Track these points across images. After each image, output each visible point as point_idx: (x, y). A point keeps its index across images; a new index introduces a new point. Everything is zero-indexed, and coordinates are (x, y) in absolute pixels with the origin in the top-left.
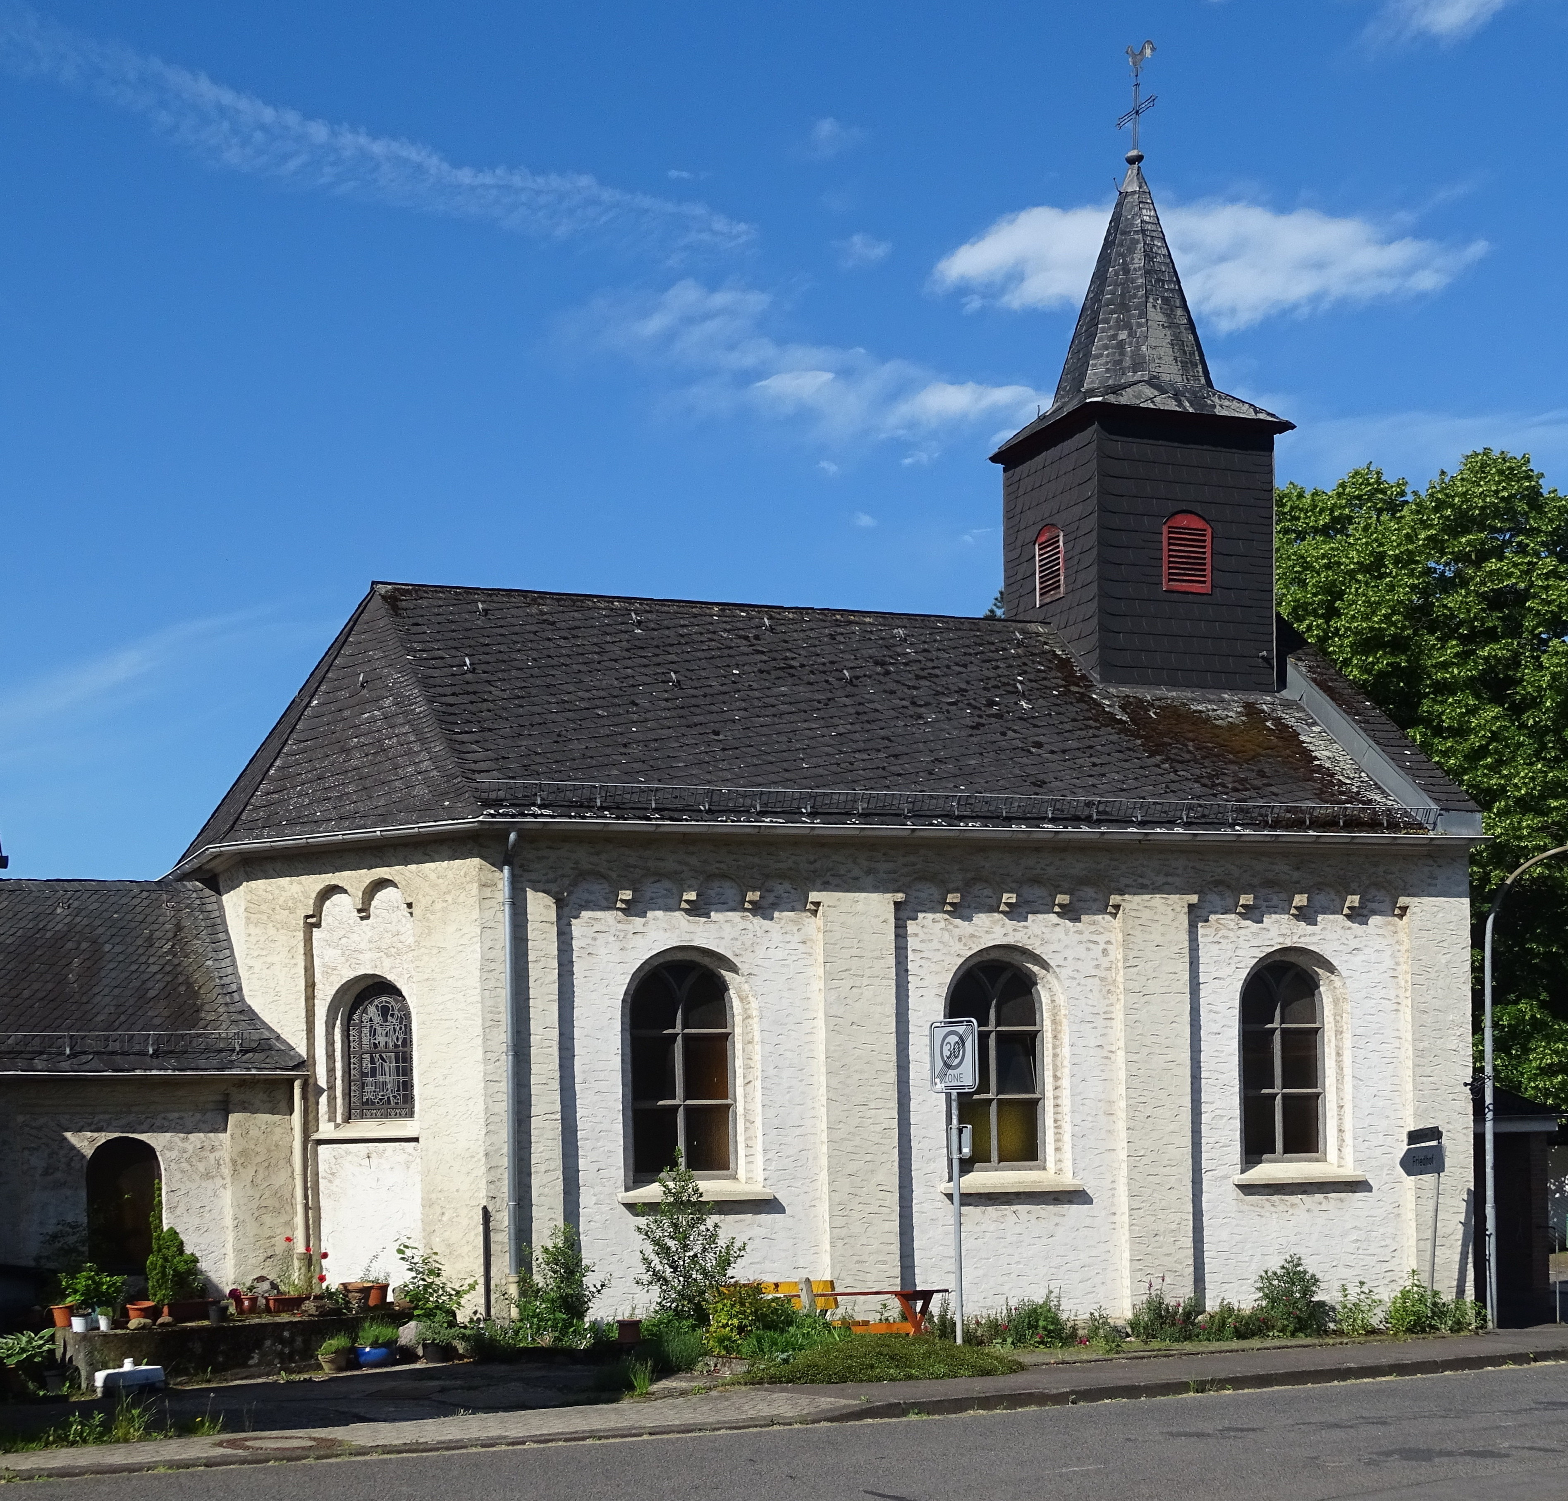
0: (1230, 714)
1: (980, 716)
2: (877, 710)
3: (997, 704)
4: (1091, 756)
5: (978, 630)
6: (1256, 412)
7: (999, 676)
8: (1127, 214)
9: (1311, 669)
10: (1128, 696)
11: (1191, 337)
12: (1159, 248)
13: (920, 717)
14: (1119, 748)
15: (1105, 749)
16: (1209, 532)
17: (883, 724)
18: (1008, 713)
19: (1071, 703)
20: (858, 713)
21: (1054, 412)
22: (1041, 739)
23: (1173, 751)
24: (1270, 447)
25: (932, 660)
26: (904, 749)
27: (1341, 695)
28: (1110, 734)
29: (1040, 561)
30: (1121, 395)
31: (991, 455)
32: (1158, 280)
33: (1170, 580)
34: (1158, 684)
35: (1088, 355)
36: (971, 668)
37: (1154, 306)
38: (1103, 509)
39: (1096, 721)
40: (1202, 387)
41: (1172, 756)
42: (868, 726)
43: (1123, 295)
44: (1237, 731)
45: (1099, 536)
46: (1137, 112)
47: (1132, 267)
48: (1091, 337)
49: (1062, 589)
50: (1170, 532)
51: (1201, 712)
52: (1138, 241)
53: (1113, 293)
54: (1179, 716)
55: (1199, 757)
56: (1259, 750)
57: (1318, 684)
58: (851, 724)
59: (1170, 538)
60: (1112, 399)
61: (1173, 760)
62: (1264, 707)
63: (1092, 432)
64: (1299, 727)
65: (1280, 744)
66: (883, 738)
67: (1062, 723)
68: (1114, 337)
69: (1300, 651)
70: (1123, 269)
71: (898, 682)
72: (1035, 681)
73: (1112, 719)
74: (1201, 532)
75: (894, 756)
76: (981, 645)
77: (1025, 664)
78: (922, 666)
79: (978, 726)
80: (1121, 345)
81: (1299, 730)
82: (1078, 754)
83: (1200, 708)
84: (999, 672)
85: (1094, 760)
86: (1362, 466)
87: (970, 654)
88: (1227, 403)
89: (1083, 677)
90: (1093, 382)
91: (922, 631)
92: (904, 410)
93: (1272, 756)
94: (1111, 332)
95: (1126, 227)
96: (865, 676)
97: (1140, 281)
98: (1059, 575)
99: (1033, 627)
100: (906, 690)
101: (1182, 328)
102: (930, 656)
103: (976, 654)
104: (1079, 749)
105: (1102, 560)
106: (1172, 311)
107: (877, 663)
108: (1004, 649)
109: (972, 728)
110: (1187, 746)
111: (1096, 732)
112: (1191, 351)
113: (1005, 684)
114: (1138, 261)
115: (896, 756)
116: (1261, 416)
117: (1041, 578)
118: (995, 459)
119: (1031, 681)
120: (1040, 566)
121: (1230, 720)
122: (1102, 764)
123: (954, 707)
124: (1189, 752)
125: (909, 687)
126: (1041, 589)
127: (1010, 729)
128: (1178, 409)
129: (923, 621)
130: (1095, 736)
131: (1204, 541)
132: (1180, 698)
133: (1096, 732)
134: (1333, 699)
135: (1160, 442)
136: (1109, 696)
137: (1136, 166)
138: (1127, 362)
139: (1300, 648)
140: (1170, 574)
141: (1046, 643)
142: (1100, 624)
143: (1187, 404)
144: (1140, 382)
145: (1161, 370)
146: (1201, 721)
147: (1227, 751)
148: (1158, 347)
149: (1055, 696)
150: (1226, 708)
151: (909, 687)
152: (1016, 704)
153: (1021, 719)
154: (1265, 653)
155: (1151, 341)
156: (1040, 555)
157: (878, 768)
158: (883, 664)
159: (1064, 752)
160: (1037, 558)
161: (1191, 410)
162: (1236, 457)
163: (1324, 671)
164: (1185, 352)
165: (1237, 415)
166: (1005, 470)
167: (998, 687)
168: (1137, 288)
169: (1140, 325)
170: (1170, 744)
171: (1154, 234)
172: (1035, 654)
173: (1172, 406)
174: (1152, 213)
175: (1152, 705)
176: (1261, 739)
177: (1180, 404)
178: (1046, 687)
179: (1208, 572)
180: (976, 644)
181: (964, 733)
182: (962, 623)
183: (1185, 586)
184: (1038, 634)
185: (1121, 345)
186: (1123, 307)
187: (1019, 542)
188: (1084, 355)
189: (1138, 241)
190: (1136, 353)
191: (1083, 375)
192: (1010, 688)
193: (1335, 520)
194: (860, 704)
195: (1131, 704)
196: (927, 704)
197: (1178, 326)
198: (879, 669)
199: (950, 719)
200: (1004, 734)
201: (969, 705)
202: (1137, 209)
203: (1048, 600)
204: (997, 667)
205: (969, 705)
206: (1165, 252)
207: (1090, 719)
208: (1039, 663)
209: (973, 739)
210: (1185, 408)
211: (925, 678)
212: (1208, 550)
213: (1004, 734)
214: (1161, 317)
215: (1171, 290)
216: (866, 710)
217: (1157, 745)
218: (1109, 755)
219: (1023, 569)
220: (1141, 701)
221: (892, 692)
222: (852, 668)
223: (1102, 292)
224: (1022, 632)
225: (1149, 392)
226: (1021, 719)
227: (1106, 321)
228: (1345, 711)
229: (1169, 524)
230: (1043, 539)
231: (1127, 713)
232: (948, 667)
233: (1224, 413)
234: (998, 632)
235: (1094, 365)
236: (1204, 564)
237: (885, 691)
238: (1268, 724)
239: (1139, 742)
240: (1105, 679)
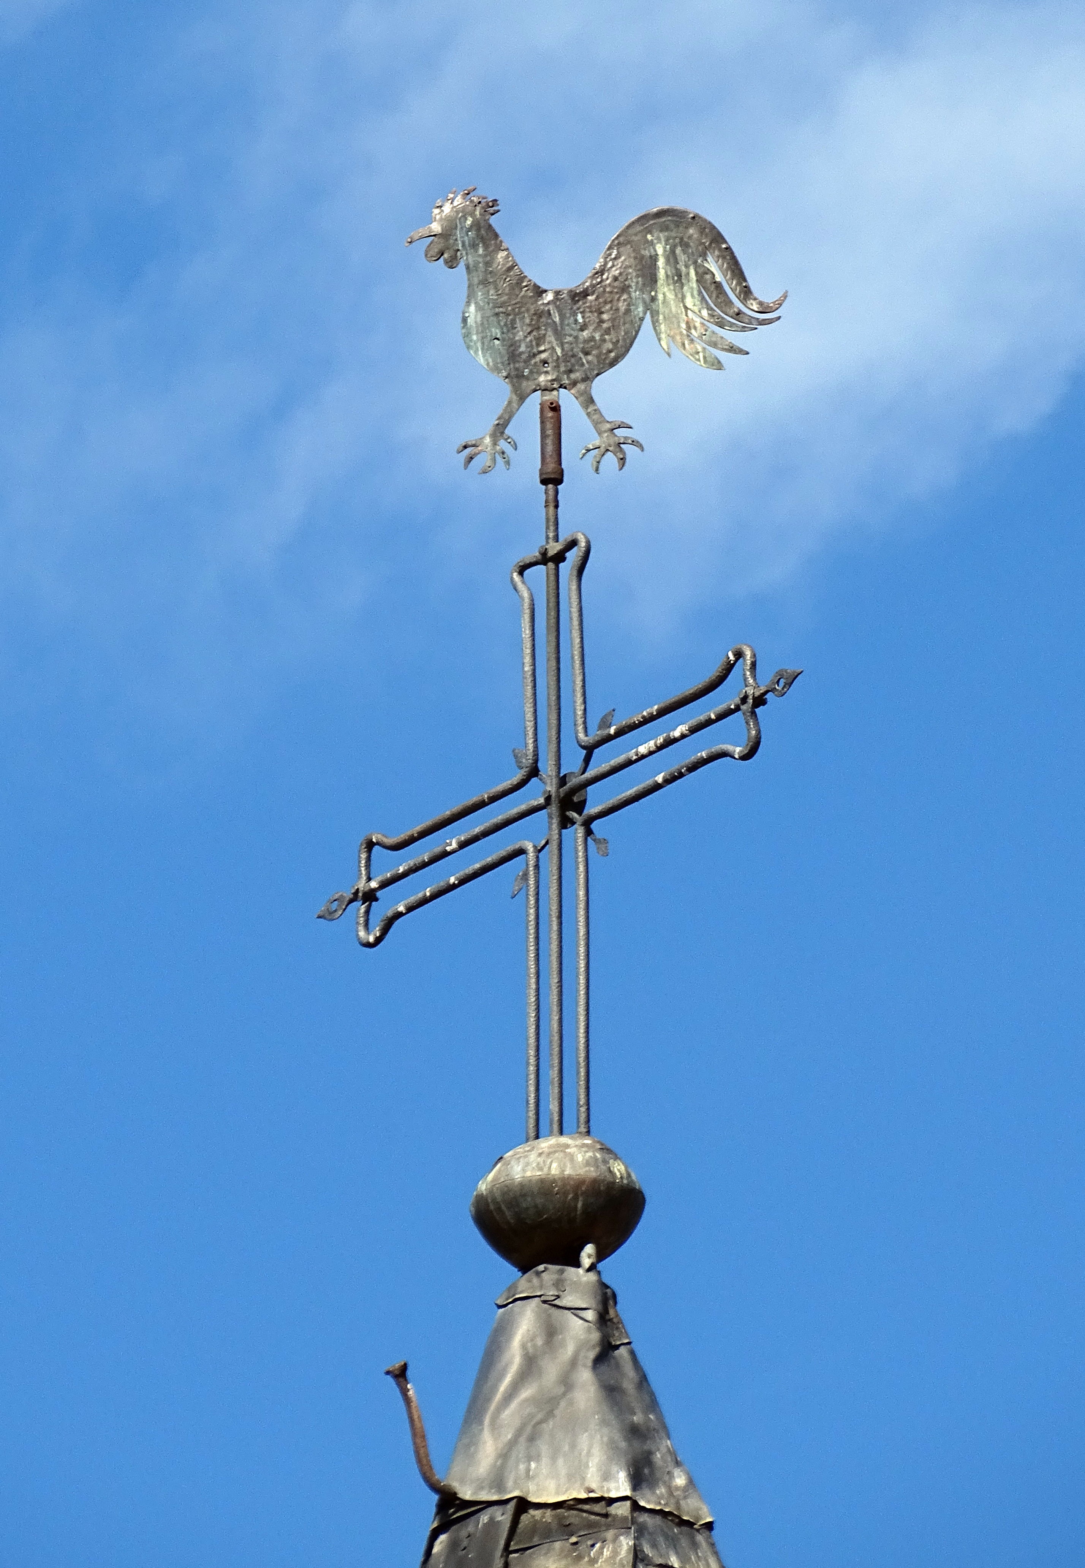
137: (578, 1281)
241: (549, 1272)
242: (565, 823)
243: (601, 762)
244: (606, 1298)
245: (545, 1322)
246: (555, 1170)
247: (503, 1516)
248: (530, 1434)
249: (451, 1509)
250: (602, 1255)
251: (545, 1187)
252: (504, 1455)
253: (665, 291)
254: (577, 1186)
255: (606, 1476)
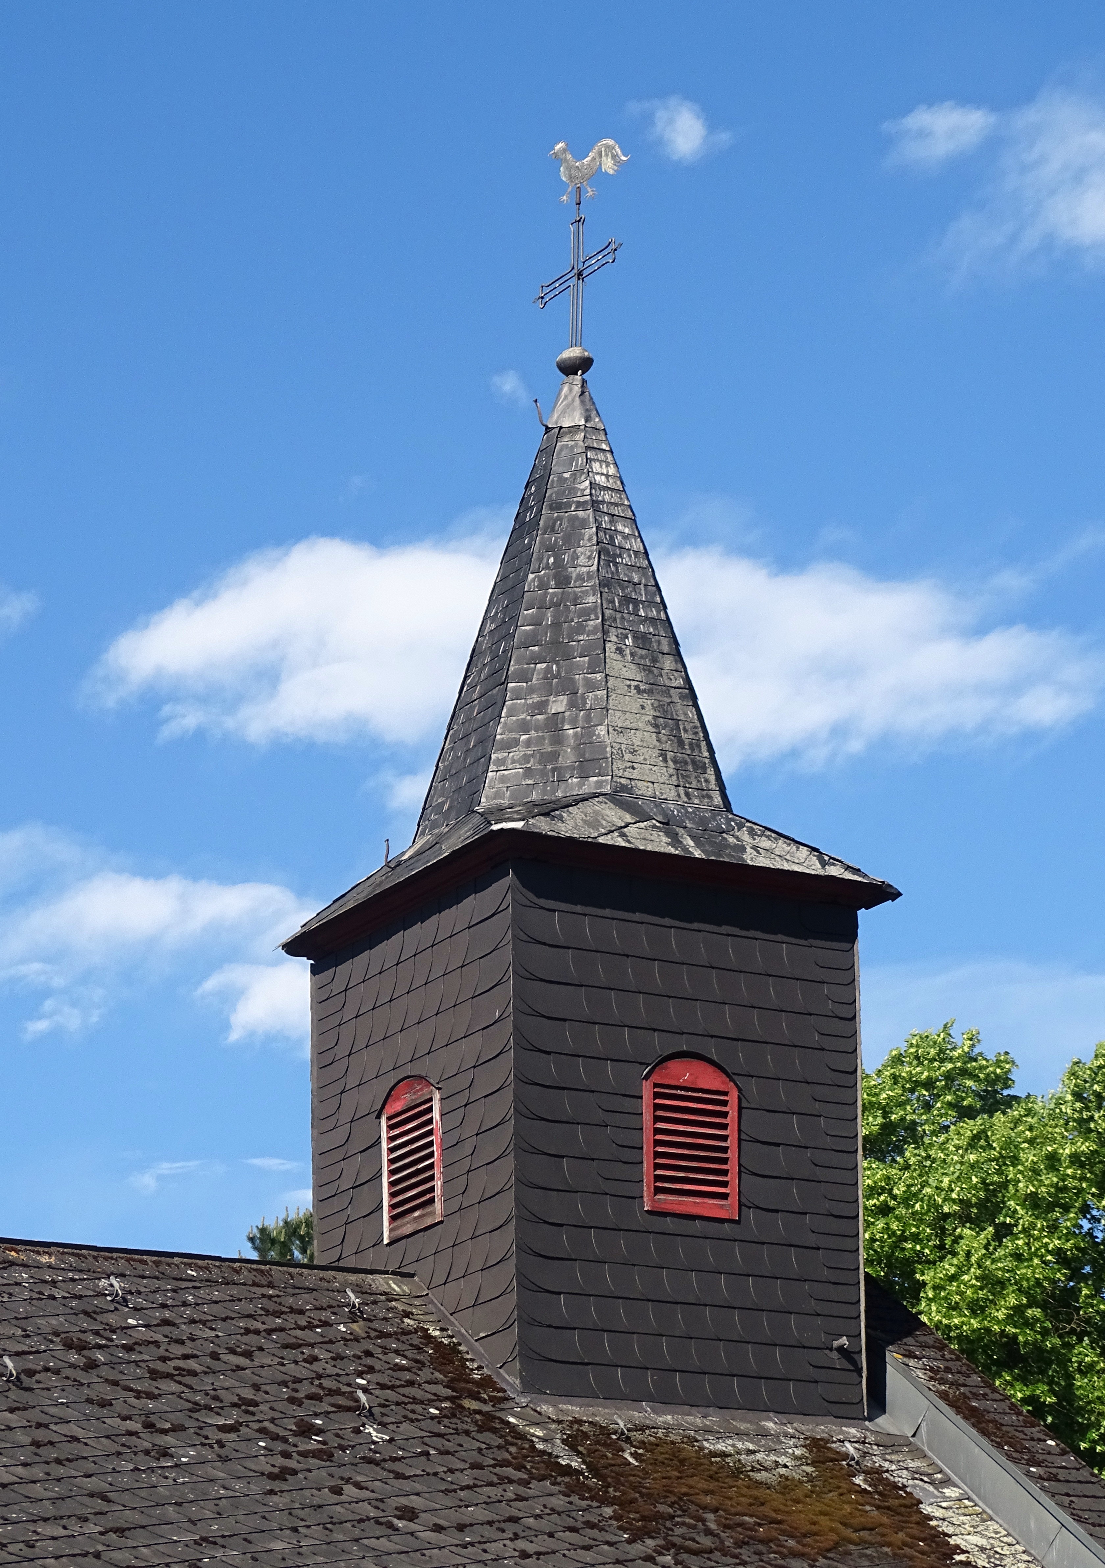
0: (783, 1460)
1: (286, 1455)
2: (74, 1439)
3: (319, 1431)
4: (516, 1537)
5: (271, 1285)
6: (824, 864)
7: (319, 1377)
8: (561, 469)
9: (934, 1374)
10: (580, 1422)
11: (692, 714)
12: (626, 537)
13: (165, 1453)
14: (570, 1522)
15: (544, 1525)
16: (733, 1098)
17: (90, 1467)
18: (343, 1449)
19: (467, 1433)
20: (36, 1444)
21: (419, 853)
22: (415, 1502)
23: (678, 1531)
24: (850, 934)
25: (182, 1342)
26: (137, 1518)
27: (999, 1425)
28: (547, 1495)
29: (391, 1150)
30: (561, 819)
31: (286, 937)
32: (627, 600)
33: (658, 1190)
34: (636, 1398)
35: (487, 742)
36: (260, 1359)
37: (620, 651)
38: (526, 1045)
39: (519, 1468)
40: (716, 812)
41: (678, 1541)
42: (61, 1471)
43: (556, 625)
44: (799, 1493)
45: (517, 1098)
46: (580, 274)
47: (574, 573)
48: (494, 707)
49: (438, 1205)
50: (657, 1095)
51: (724, 1455)
52: (584, 524)
53: (536, 622)
54: (682, 1462)
55: (729, 1543)
56: (848, 1532)
57: (951, 1404)
58: (25, 1465)
59: (657, 1107)
60: (542, 825)
61: (680, 1549)
62: (850, 1448)
63: (502, 890)
64: (917, 1488)
65: (885, 1520)
66: (91, 1495)
67: (451, 1471)
68: (541, 707)
69: (909, 1340)
70: (555, 577)
71: (115, 1383)
72: (392, 1388)
73: (553, 1469)
74: (718, 1098)
75: (116, 1530)
76: (278, 1314)
77: (368, 1354)
78: (161, 1352)
79: (283, 1474)
80: (554, 724)
81: (918, 1494)
82: (489, 1532)
83: (721, 1446)
84: (317, 1367)
85: (522, 1544)
86: (934, 1030)
87: (257, 1332)
88: (765, 843)
89: (487, 1382)
90: (497, 795)
91: (156, 1283)
92: (44, 923)
93: (871, 1544)
94: (535, 698)
95: (561, 493)
96: (47, 1369)
97: (591, 599)
98: (432, 1178)
99: (379, 1282)
100: (133, 1401)
101: (675, 695)
102: (175, 1333)
103: (270, 1332)
104: (490, 1523)
105: (524, 1148)
106: (654, 660)
107: (69, 1345)
108: (325, 1324)
109: (272, 1477)
110: (704, 1521)
111: (522, 1490)
112: (689, 745)
113: (331, 1392)
114: (585, 561)
115: (120, 1531)
116: (835, 871)
117: (392, 1184)
118: (294, 947)
119: (383, 1387)
120: (392, 1161)
121: (783, 1471)
122: (539, 1554)
123: (233, 1436)
124: (708, 1532)
125: (138, 1395)
126: (393, 1207)
127: (348, 1481)
128: (671, 850)
129: (157, 1264)
130: (520, 1498)
131: (725, 1115)
132: (680, 1426)
133: (522, 1490)
134: (984, 1432)
135: (637, 916)
136: (543, 1419)
137: (578, 378)
138: (568, 757)
139: (909, 1334)
140: (658, 1178)
141: (407, 1315)
142: (520, 1274)
143: (689, 842)
144: (595, 796)
145: (635, 774)
146: (726, 1472)
147: (783, 1532)
148: (627, 725)
149: (433, 1417)
150: (772, 1448)
151: (138, 1395)
152: (357, 1431)
153: (370, 1461)
154: (844, 1340)
155: (616, 718)
156: (391, 1139)
157: (85, 1554)
158: (81, 1347)
159: (461, 1528)
160: (384, 1145)
161: (697, 854)
162: (787, 952)
163: (962, 1380)
164: (681, 743)
165: (786, 867)
166: (314, 971)
167: (320, 1399)
168: (586, 613)
169: (592, 686)
170: (672, 1517)
171: (615, 511)
172: (388, 1335)
173: (660, 843)
174: (612, 470)
175: (628, 1440)
176: (848, 1508)
177: (675, 840)
178: (415, 1400)
179: (732, 1178)
180: (267, 1312)
181: (255, 1489)
182: (237, 1272)
183: (688, 1205)
184: (390, 1297)
185: (554, 724)
186: (558, 650)
187: (345, 1115)
188: (481, 742)
189: (584, 524)
190: (586, 739)
191: (476, 784)
192: (341, 1401)
193: (888, 1128)
194: (39, 1425)
195: (586, 1436)
196: (177, 1429)
197: (667, 690)
198: (74, 1357)
199: (225, 1460)
200: (337, 1491)
201: (262, 1430)
202: (581, 460)
203: (408, 1229)
204: (316, 1359)
205: (262, 1430)
206: (637, 545)
207: (505, 1464)
208: (397, 1352)
209: (275, 1498)
210: (686, 849)
211: (169, 1376)
212: (731, 1132)
213: (337, 1491)
214: (631, 672)
215: (653, 621)
216: (55, 1438)
217: (643, 1518)
218: (551, 1535)
219: (351, 1171)
220: (605, 1431)
221: (104, 1404)
222: (18, 1354)
223: (514, 619)
224: (360, 1290)
225: (614, 815)
226: (370, 1461)
227: (525, 677)
228: (1009, 1457)
229: (654, 1078)
230: (398, 1106)
231: (579, 1453)
232: (215, 1356)
233: (762, 861)
234: (310, 1290)
235: (502, 762)
236: (725, 1161)
237: (89, 1401)
238: (859, 1480)
239: (608, 1511)
240: (528, 1387)
241: (571, 377)
242: (579, 279)
243: (586, 265)
244: (584, 382)
245: (571, 386)
246: (572, 355)
247: (557, 430)
248: (564, 412)
249: (548, 429)
250: (583, 373)
251: (570, 358)
252: (558, 417)
253: (604, 158)
254: (576, 358)
255: (579, 420)
